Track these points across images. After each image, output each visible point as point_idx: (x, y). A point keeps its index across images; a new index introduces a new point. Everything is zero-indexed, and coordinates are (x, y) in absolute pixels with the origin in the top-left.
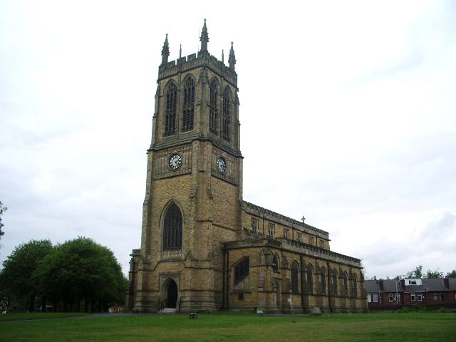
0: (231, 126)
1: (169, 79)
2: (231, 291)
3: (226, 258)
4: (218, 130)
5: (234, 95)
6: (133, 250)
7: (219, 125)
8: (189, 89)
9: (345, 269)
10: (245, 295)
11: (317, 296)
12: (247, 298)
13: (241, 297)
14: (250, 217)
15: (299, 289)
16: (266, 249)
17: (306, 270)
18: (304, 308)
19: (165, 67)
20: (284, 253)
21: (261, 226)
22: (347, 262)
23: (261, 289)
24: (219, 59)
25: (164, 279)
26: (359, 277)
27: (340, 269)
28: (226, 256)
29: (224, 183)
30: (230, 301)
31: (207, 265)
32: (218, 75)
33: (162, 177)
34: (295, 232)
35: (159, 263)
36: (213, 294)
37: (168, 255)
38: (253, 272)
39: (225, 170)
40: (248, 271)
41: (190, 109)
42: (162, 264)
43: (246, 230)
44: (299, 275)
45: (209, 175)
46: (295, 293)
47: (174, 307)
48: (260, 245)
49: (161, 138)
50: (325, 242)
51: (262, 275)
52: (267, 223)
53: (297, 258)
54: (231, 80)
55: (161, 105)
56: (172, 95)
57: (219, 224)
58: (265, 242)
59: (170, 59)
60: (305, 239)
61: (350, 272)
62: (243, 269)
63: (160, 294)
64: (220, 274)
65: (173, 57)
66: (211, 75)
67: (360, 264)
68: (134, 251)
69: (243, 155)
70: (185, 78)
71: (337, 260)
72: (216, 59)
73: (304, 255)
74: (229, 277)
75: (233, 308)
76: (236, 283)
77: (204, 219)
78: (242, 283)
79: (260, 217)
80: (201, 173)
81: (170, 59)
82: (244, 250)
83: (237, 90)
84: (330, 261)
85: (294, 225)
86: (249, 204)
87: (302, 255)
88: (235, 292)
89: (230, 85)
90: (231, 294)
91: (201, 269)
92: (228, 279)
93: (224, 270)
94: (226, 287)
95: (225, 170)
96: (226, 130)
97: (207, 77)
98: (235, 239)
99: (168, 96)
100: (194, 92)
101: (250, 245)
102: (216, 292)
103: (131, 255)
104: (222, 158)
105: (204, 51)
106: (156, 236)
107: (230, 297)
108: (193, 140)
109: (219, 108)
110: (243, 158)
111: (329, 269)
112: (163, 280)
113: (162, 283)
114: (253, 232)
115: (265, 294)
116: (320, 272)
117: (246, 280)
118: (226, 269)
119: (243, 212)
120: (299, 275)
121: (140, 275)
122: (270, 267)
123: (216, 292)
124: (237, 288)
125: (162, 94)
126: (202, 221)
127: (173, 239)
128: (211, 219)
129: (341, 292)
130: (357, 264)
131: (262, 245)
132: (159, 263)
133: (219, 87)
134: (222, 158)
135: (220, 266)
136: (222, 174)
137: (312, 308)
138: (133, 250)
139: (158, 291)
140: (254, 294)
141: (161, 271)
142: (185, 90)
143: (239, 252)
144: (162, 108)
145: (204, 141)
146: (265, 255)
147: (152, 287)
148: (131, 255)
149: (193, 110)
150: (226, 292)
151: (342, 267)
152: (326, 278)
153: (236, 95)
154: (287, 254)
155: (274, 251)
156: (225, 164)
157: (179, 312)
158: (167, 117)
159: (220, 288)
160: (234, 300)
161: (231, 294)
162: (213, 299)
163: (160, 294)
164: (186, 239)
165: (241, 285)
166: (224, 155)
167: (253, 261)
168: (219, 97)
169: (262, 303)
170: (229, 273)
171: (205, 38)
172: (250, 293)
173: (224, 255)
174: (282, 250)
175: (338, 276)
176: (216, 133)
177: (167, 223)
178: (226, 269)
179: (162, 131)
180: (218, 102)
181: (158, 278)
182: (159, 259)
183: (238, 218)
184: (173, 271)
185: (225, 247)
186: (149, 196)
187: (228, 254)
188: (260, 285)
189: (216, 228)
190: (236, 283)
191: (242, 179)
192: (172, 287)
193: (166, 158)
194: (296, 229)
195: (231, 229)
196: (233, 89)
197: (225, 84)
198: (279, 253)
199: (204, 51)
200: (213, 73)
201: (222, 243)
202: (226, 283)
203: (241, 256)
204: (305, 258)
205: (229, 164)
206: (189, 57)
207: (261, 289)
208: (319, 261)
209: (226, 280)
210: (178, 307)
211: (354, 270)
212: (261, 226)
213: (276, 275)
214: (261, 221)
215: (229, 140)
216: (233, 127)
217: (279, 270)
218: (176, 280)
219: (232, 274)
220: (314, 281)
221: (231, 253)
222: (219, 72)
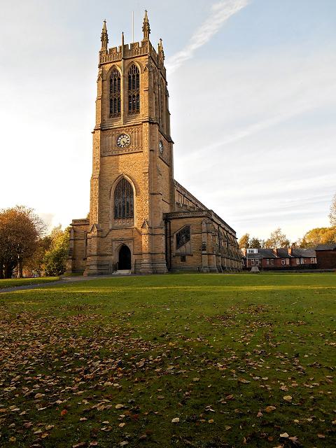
1: (112, 64)
2: (173, 254)
8: (134, 76)
13: (183, 259)
19: (106, 55)
22: (219, 223)
25: (117, 245)
28: (168, 223)
33: (111, 154)
35: (110, 230)
37: (120, 223)
41: (136, 95)
42: (114, 232)
43: (178, 204)
47: (129, 268)
49: (106, 119)
55: (105, 88)
56: (115, 80)
59: (110, 46)
62: (184, 235)
63: (113, 257)
65: (115, 43)
70: (129, 65)
76: (178, 247)
77: (155, 192)
78: (183, 247)
81: (110, 46)
82: (185, 220)
88: (177, 255)
93: (168, 235)
99: (111, 81)
100: (138, 79)
105: (146, 42)
108: (144, 122)
112: (116, 245)
113: (115, 248)
117: (188, 244)
124: (179, 251)
125: (105, 79)
127: (124, 211)
132: (110, 230)
141: (113, 238)
143: (180, 221)
145: (153, 123)
146: (206, 223)
150: (168, 255)
157: (135, 273)
158: (111, 100)
163: (115, 258)
165: (183, 249)
169: (205, 263)
171: (146, 29)
173: (166, 223)
177: (117, 194)
178: (168, 236)
179: (107, 112)
182: (110, 227)
184: (125, 237)
190: (178, 247)
192: (125, 253)
193: (114, 137)
199: (146, 42)
206: (132, 45)
209: (168, 245)
210: (133, 269)
218: (130, 245)
219: (174, 240)
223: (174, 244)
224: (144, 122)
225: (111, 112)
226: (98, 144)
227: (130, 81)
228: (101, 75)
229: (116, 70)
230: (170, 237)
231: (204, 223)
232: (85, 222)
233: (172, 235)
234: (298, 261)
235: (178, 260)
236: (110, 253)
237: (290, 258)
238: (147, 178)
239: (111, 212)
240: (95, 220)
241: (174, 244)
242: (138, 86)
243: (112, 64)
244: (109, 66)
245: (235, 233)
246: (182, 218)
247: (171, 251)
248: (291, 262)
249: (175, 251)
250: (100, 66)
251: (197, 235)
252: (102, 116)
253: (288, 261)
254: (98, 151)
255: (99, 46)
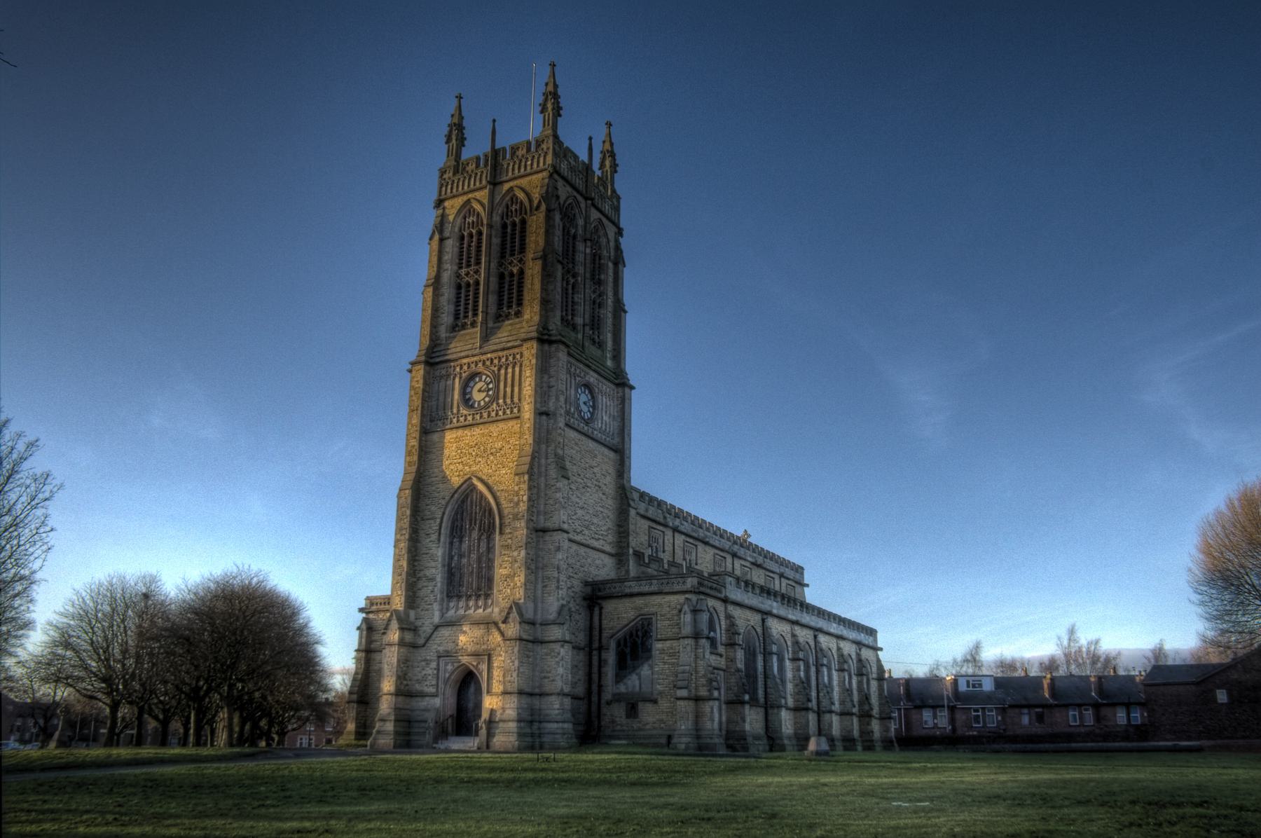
0: (607, 315)
1: (465, 198)
2: (607, 696)
3: (596, 619)
4: (579, 321)
5: (612, 244)
6: (368, 598)
7: (580, 309)
9: (848, 648)
10: (641, 705)
11: (796, 709)
12: (649, 716)
13: (632, 711)
14: (645, 524)
15: (761, 693)
16: (694, 598)
17: (774, 648)
18: (770, 738)
20: (731, 608)
21: (668, 548)
23: (684, 693)
24: (583, 156)
25: (449, 667)
26: (874, 669)
27: (839, 649)
29: (592, 444)
30: (606, 720)
31: (556, 633)
32: (581, 195)
34: (737, 563)
35: (437, 627)
36: (567, 701)
38: (662, 651)
39: (592, 414)
40: (648, 651)
41: (515, 270)
43: (639, 555)
44: (760, 659)
45: (561, 425)
46: (754, 702)
48: (677, 588)
49: (443, 333)
50: (798, 588)
51: (686, 657)
52: (680, 539)
53: (755, 619)
54: (607, 208)
55: (446, 257)
57: (578, 538)
58: (691, 582)
60: (758, 577)
61: (858, 655)
63: (437, 702)
64: (582, 656)
66: (564, 191)
67: (875, 640)
68: (371, 601)
69: (632, 382)
71: (834, 628)
72: (576, 157)
73: (769, 614)
74: (601, 663)
75: (611, 737)
76: (619, 678)
78: (634, 677)
79: (666, 526)
80: (544, 417)
82: (639, 601)
83: (620, 232)
84: (820, 630)
85: (736, 548)
86: (643, 495)
87: (766, 614)
88: (618, 698)
89: (604, 220)
90: (609, 703)
91: (542, 642)
92: (600, 667)
93: (591, 647)
94: (595, 687)
95: (592, 414)
96: (595, 324)
97: (558, 197)
98: (613, 575)
99: (462, 238)
100: (523, 230)
101: (654, 588)
102: (575, 697)
103: (361, 610)
104: (587, 386)
106: (433, 564)
107: (604, 710)
109: (580, 269)
110: (632, 388)
111: (819, 650)
114: (655, 559)
115: (691, 703)
116: (801, 655)
117: (645, 670)
118: (596, 645)
119: (632, 512)
120: (760, 659)
121: (390, 659)
122: (703, 642)
123: (575, 697)
124: (622, 688)
125: (447, 234)
126: (544, 531)
128: (565, 526)
129: (842, 703)
130: (869, 640)
131: (684, 588)
132: (437, 627)
133: (581, 222)
134: (587, 386)
135: (581, 638)
136: (587, 423)
137: (625, 684)
138: (368, 598)
139: (435, 695)
140: (664, 704)
141: (441, 649)
142: (504, 226)
144: (448, 266)
145: (550, 342)
147: (418, 687)
148: (361, 610)
149: (522, 272)
150: (595, 698)
151: (842, 644)
152: (813, 669)
153: (618, 248)
154: (736, 612)
155: (711, 602)
156: (593, 397)
158: (459, 287)
159: (580, 690)
160: (618, 713)
161: (609, 703)
162: (568, 715)
164: (504, 572)
165: (632, 683)
166: (592, 378)
167: (662, 627)
168: (580, 246)
169: (684, 726)
170: (604, 655)
172: (655, 702)
174: (725, 601)
175: (788, 656)
176: (574, 328)
178: (596, 645)
179: (446, 319)
180: (580, 257)
181: (434, 665)
182: (436, 619)
183: (619, 526)
185: (593, 590)
186: (414, 469)
187: (601, 608)
188: (680, 684)
189: (575, 547)
190: (619, 678)
191: (629, 435)
194: (740, 558)
195: (603, 552)
196: (611, 231)
197: (595, 215)
198: (719, 606)
200: (569, 189)
201: (586, 584)
202: (595, 677)
203: (632, 614)
204: (823, 639)
205: (603, 401)
207: (684, 693)
208: (798, 630)
209: (595, 669)
211: (866, 653)
212: (668, 548)
213: (713, 660)
214: (669, 533)
215: (600, 345)
216: (610, 315)
217: (721, 649)
219: (611, 657)
220: (789, 675)
221: (609, 606)
222: (581, 187)
223: (610, 671)
224: (525, 340)
225: (457, 317)
226: (418, 402)
227: (504, 235)
228: (440, 227)
229: (472, 211)
230: (600, 648)
231: (686, 608)
232: (387, 600)
233: (604, 641)
234: (1121, 716)
235: (619, 712)
236: (432, 690)
237: (1097, 706)
238: (525, 486)
239: (439, 578)
240: (399, 604)
241: (610, 671)
242: (523, 249)
243: (465, 198)
244: (459, 201)
245: (872, 632)
246: (632, 595)
247: (600, 686)
248: (1098, 718)
249: (610, 687)
250: (439, 203)
251: (668, 644)
252: (434, 326)
253: (1089, 714)
254: (416, 420)
255: (440, 156)
